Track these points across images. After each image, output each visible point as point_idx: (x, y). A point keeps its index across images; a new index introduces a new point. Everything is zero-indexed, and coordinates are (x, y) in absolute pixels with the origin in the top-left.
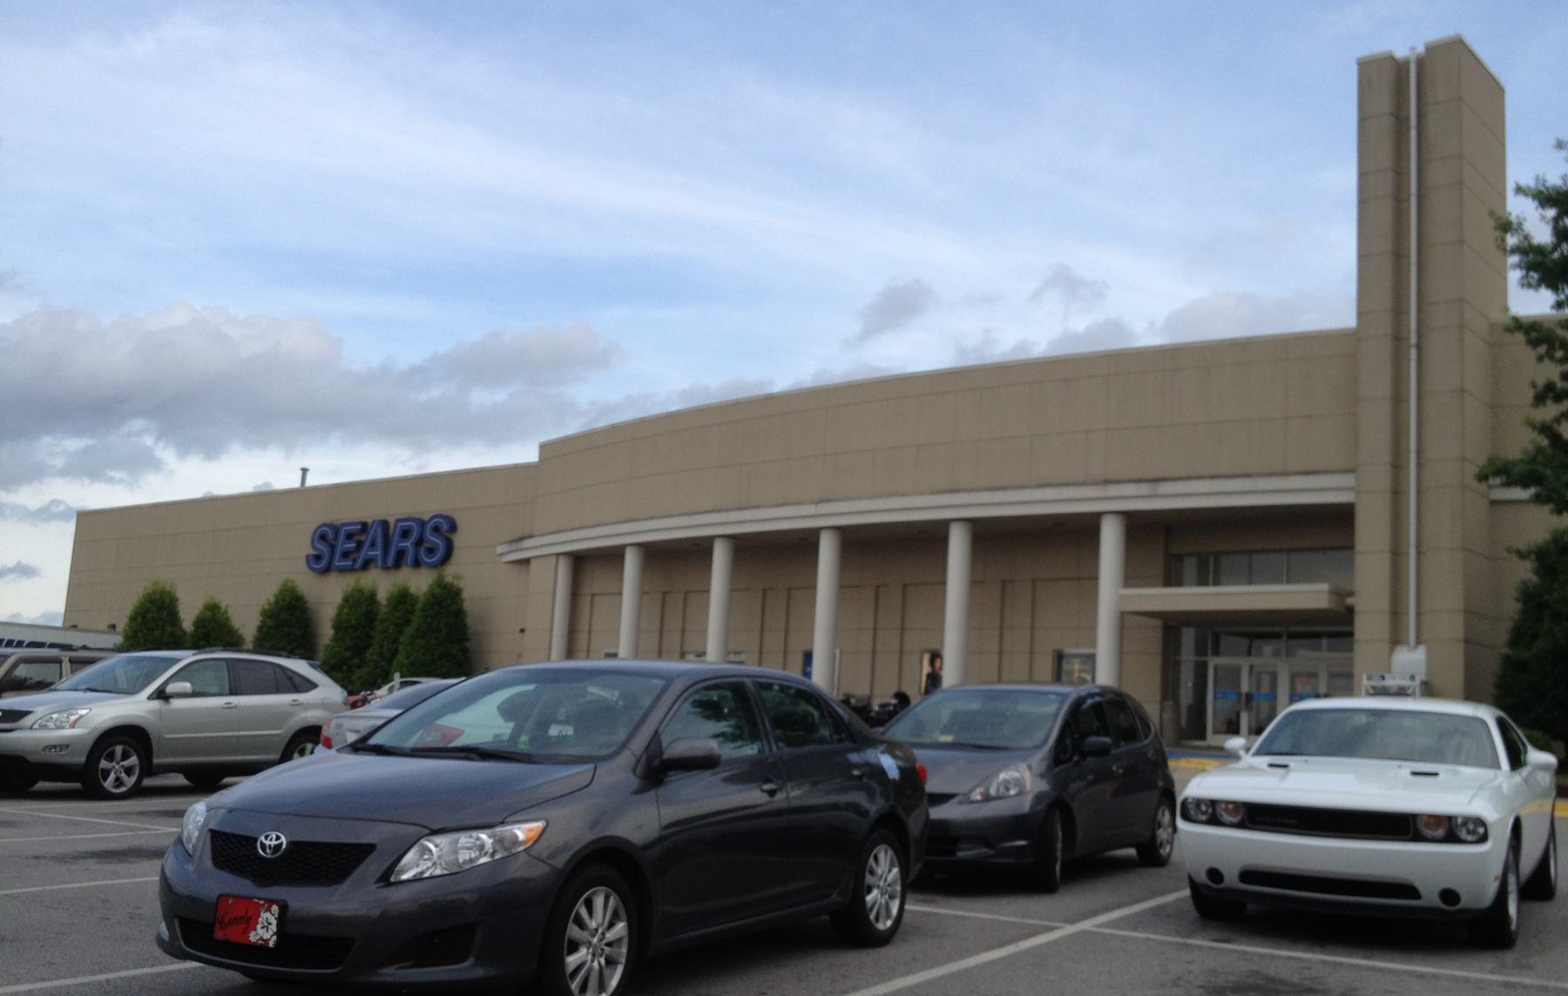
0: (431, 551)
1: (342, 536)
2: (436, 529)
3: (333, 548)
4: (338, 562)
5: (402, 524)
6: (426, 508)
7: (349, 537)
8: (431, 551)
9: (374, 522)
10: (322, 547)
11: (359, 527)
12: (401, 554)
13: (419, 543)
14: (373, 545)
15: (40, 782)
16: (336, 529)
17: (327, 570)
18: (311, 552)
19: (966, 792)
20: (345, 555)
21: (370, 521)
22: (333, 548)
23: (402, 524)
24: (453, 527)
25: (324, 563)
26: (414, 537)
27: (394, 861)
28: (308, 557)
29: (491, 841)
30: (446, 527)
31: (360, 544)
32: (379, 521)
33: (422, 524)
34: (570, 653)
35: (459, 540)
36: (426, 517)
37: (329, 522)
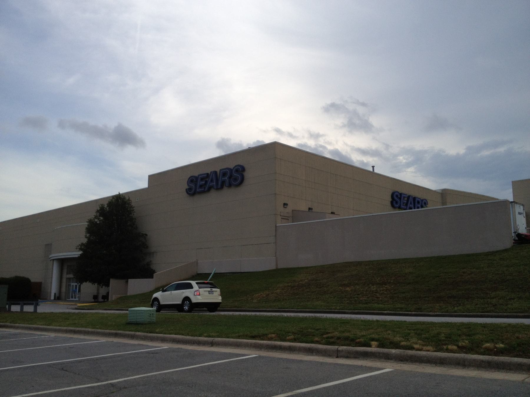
0: (236, 180)
1: (199, 180)
2: (237, 171)
3: (196, 185)
4: (198, 189)
5: (200, 176)
6: (231, 165)
7: (202, 179)
8: (236, 180)
9: (211, 172)
10: (192, 185)
11: (206, 175)
12: (223, 183)
13: (230, 177)
14: (212, 181)
15: (154, 294)
16: (197, 178)
17: (193, 194)
18: (187, 187)
19: (179, 302)
20: (201, 186)
21: (209, 172)
22: (196, 185)
23: (200, 176)
24: (243, 169)
25: (192, 192)
26: (228, 174)
27: (240, 354)
28: (186, 189)
29: (211, 335)
30: (240, 170)
31: (206, 182)
32: (213, 171)
33: (231, 170)
34: (444, 203)
35: (247, 174)
36: (232, 167)
37: (242, 165)
